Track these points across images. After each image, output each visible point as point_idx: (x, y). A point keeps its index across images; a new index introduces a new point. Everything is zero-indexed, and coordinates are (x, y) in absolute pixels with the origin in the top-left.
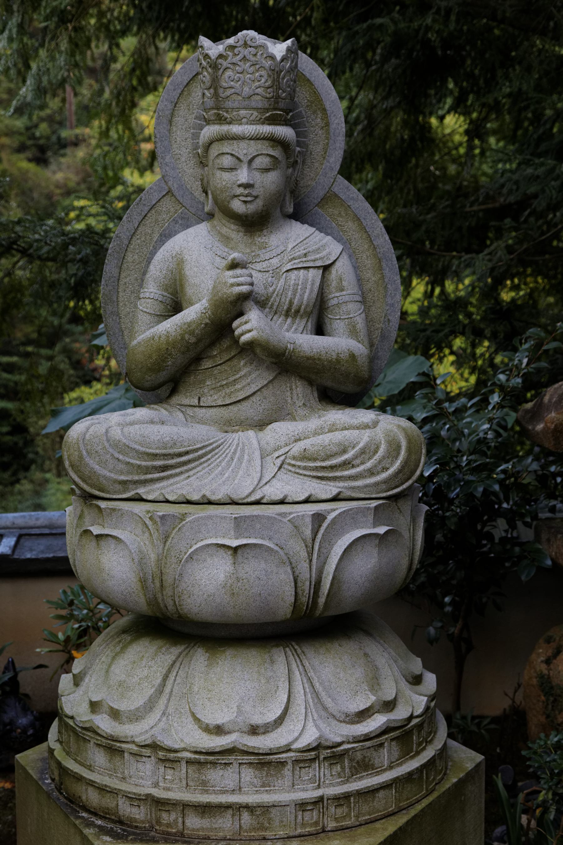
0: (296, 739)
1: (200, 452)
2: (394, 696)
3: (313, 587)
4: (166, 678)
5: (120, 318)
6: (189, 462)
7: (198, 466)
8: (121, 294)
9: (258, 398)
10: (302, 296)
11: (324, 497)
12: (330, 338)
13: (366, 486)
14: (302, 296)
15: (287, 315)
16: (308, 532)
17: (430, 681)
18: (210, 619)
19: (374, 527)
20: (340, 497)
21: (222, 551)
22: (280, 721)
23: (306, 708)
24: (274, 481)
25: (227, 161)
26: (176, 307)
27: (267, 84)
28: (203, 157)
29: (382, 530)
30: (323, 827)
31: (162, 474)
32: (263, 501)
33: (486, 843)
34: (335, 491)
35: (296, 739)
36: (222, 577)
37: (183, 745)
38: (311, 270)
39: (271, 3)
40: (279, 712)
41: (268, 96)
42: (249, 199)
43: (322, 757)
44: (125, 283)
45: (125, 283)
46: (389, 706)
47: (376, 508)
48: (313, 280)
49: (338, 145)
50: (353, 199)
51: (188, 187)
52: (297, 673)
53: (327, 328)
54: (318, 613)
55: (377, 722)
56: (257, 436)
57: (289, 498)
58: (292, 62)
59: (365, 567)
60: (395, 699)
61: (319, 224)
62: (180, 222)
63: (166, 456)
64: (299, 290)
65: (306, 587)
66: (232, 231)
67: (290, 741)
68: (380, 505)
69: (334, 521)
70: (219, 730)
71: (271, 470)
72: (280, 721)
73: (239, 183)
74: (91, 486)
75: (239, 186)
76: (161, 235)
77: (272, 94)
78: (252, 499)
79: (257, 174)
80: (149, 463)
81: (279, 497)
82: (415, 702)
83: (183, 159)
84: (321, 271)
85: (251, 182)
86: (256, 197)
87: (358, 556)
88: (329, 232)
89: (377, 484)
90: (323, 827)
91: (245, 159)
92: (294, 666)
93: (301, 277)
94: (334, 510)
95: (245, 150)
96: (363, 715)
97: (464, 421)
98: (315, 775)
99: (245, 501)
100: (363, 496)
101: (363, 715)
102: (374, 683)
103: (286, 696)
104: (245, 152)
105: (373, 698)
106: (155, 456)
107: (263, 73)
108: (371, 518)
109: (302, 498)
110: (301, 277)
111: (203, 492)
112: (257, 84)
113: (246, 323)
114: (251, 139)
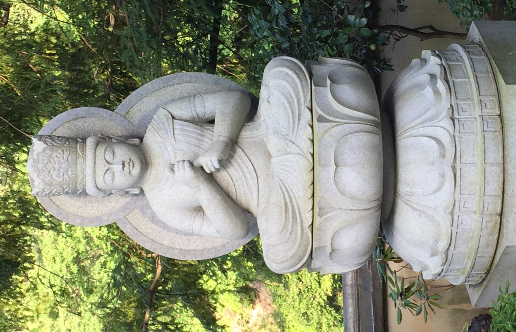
0: (448, 131)
2: (428, 75)
3: (363, 122)
5: (205, 248)
6: (290, 197)
7: (292, 192)
8: (190, 248)
9: (253, 158)
11: (310, 116)
12: (216, 115)
13: (304, 92)
15: (202, 141)
19: (327, 87)
20: (310, 107)
21: (339, 174)
22: (438, 141)
23: (432, 126)
24: (301, 146)
27: (61, 153)
28: (105, 193)
29: (329, 82)
30: (498, 115)
32: (312, 152)
33: (515, 20)
35: (448, 131)
36: (354, 174)
37: (452, 197)
38: (175, 127)
40: (434, 142)
41: (68, 152)
42: (131, 164)
43: (458, 117)
44: (184, 245)
45: (184, 245)
46: (433, 76)
47: (315, 86)
48: (181, 125)
49: (96, 112)
50: (129, 103)
51: (122, 205)
52: (413, 131)
54: (379, 120)
55: (441, 85)
56: (275, 157)
57: (310, 137)
58: (47, 138)
59: (349, 92)
60: (429, 74)
61: (145, 123)
62: (145, 211)
63: (286, 211)
64: (187, 134)
67: (448, 135)
68: (314, 84)
69: (322, 110)
70: (443, 176)
71: (294, 149)
72: (438, 141)
73: (122, 170)
74: (304, 256)
75: (124, 170)
76: (153, 223)
77: (68, 150)
79: (116, 160)
80: (291, 220)
81: (309, 143)
82: (434, 63)
83: (105, 209)
84: (175, 121)
85: (122, 163)
86: (130, 160)
87: (347, 96)
88: (150, 117)
89: (302, 86)
90: (498, 115)
92: (408, 134)
93: (179, 132)
94: (316, 110)
95: (101, 167)
96: (436, 92)
98: (468, 121)
99: (312, 163)
100: (310, 94)
101: (436, 92)
102: (420, 87)
103: (425, 138)
104: (103, 166)
105: (428, 87)
106: (286, 218)
107: (54, 155)
108: (322, 89)
110: (179, 132)
111: (307, 187)
112: (61, 159)
113: (207, 165)
114: (95, 163)
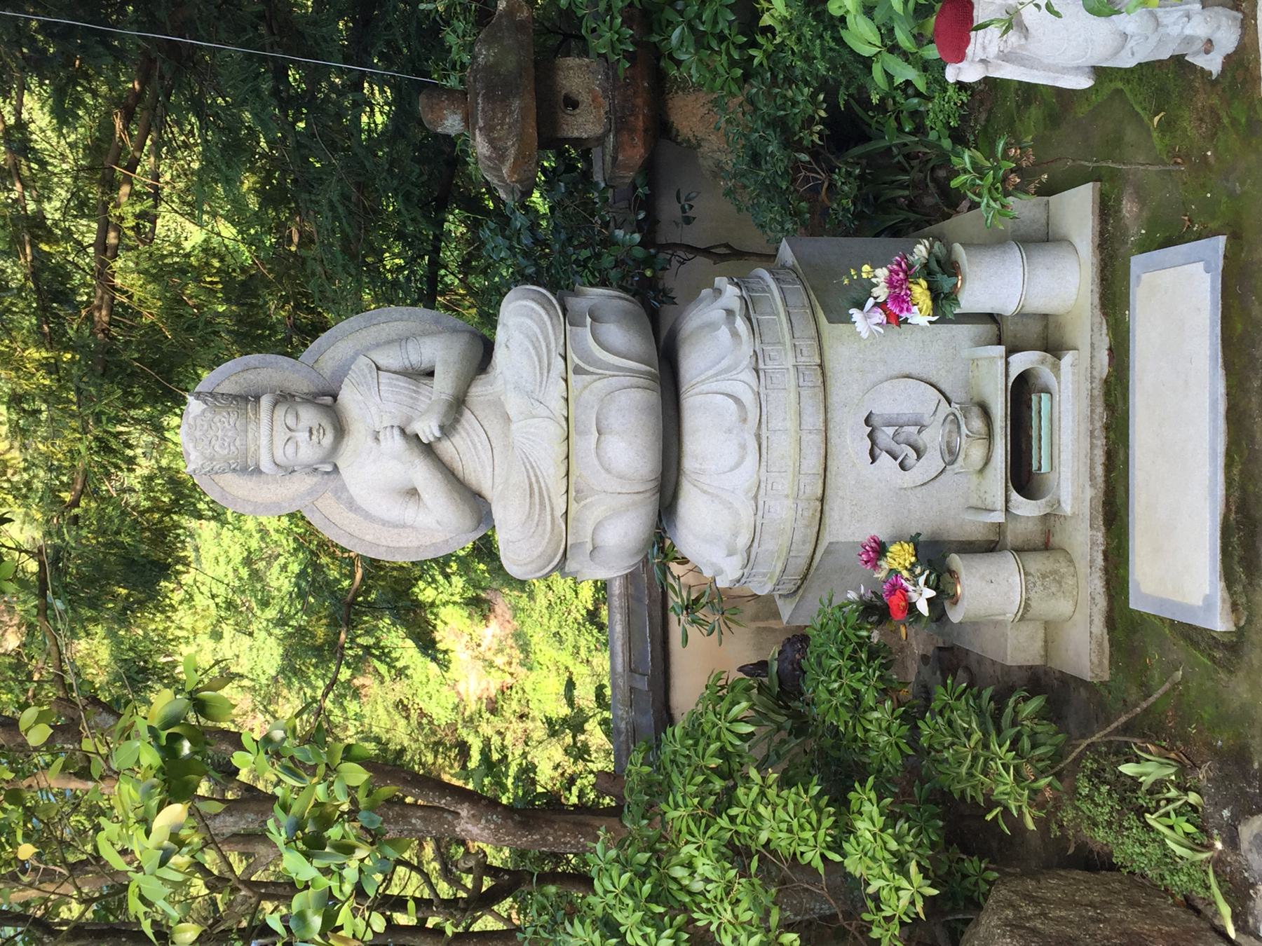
1: (533, 479)
4: (705, 492)
6: (536, 476)
10: (402, 388)
14: (402, 388)
16: (588, 378)
17: (721, 281)
18: (658, 457)
21: (602, 445)
22: (737, 400)
25: (290, 449)
26: (413, 493)
29: (589, 320)
31: (548, 508)
34: (560, 359)
36: (623, 445)
39: (502, 5)
46: (730, 313)
53: (425, 365)
55: (740, 324)
65: (634, 380)
66: (349, 444)
70: (743, 447)
72: (737, 400)
74: (555, 555)
78: (564, 423)
79: (301, 425)
81: (563, 402)
91: (289, 434)
92: (696, 390)
96: (735, 334)
97: (1008, 742)
102: (712, 326)
109: (563, 383)
